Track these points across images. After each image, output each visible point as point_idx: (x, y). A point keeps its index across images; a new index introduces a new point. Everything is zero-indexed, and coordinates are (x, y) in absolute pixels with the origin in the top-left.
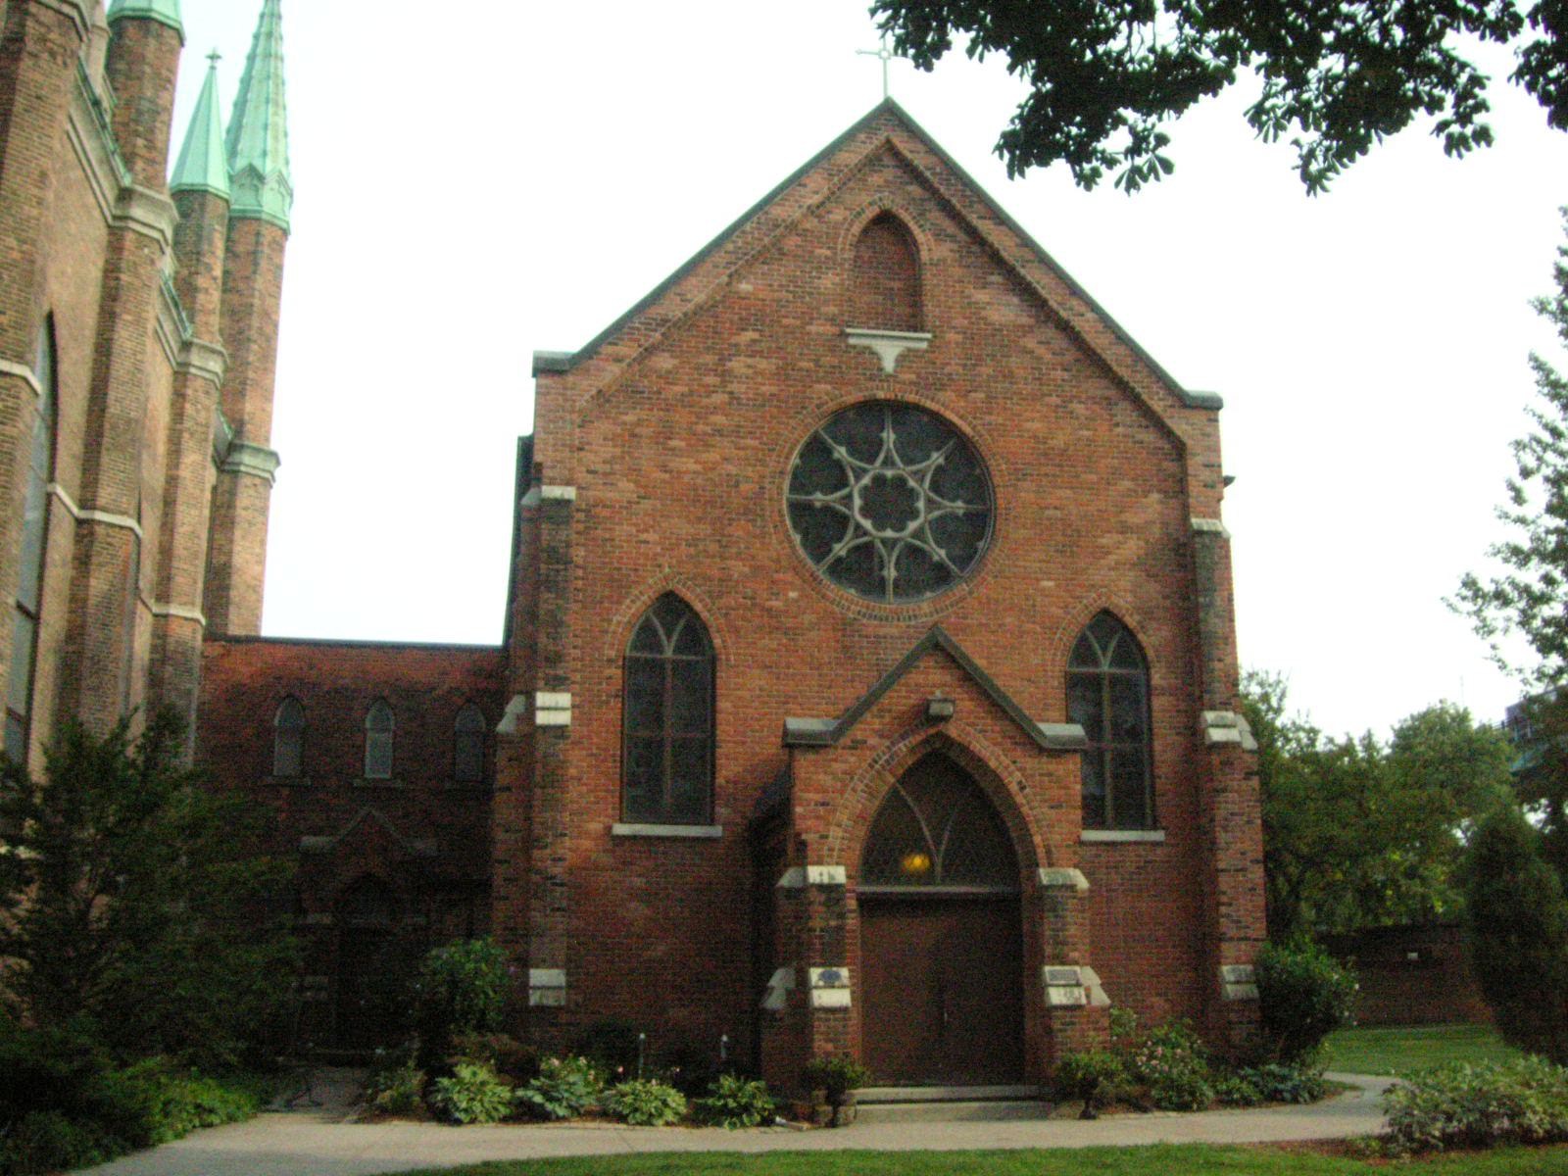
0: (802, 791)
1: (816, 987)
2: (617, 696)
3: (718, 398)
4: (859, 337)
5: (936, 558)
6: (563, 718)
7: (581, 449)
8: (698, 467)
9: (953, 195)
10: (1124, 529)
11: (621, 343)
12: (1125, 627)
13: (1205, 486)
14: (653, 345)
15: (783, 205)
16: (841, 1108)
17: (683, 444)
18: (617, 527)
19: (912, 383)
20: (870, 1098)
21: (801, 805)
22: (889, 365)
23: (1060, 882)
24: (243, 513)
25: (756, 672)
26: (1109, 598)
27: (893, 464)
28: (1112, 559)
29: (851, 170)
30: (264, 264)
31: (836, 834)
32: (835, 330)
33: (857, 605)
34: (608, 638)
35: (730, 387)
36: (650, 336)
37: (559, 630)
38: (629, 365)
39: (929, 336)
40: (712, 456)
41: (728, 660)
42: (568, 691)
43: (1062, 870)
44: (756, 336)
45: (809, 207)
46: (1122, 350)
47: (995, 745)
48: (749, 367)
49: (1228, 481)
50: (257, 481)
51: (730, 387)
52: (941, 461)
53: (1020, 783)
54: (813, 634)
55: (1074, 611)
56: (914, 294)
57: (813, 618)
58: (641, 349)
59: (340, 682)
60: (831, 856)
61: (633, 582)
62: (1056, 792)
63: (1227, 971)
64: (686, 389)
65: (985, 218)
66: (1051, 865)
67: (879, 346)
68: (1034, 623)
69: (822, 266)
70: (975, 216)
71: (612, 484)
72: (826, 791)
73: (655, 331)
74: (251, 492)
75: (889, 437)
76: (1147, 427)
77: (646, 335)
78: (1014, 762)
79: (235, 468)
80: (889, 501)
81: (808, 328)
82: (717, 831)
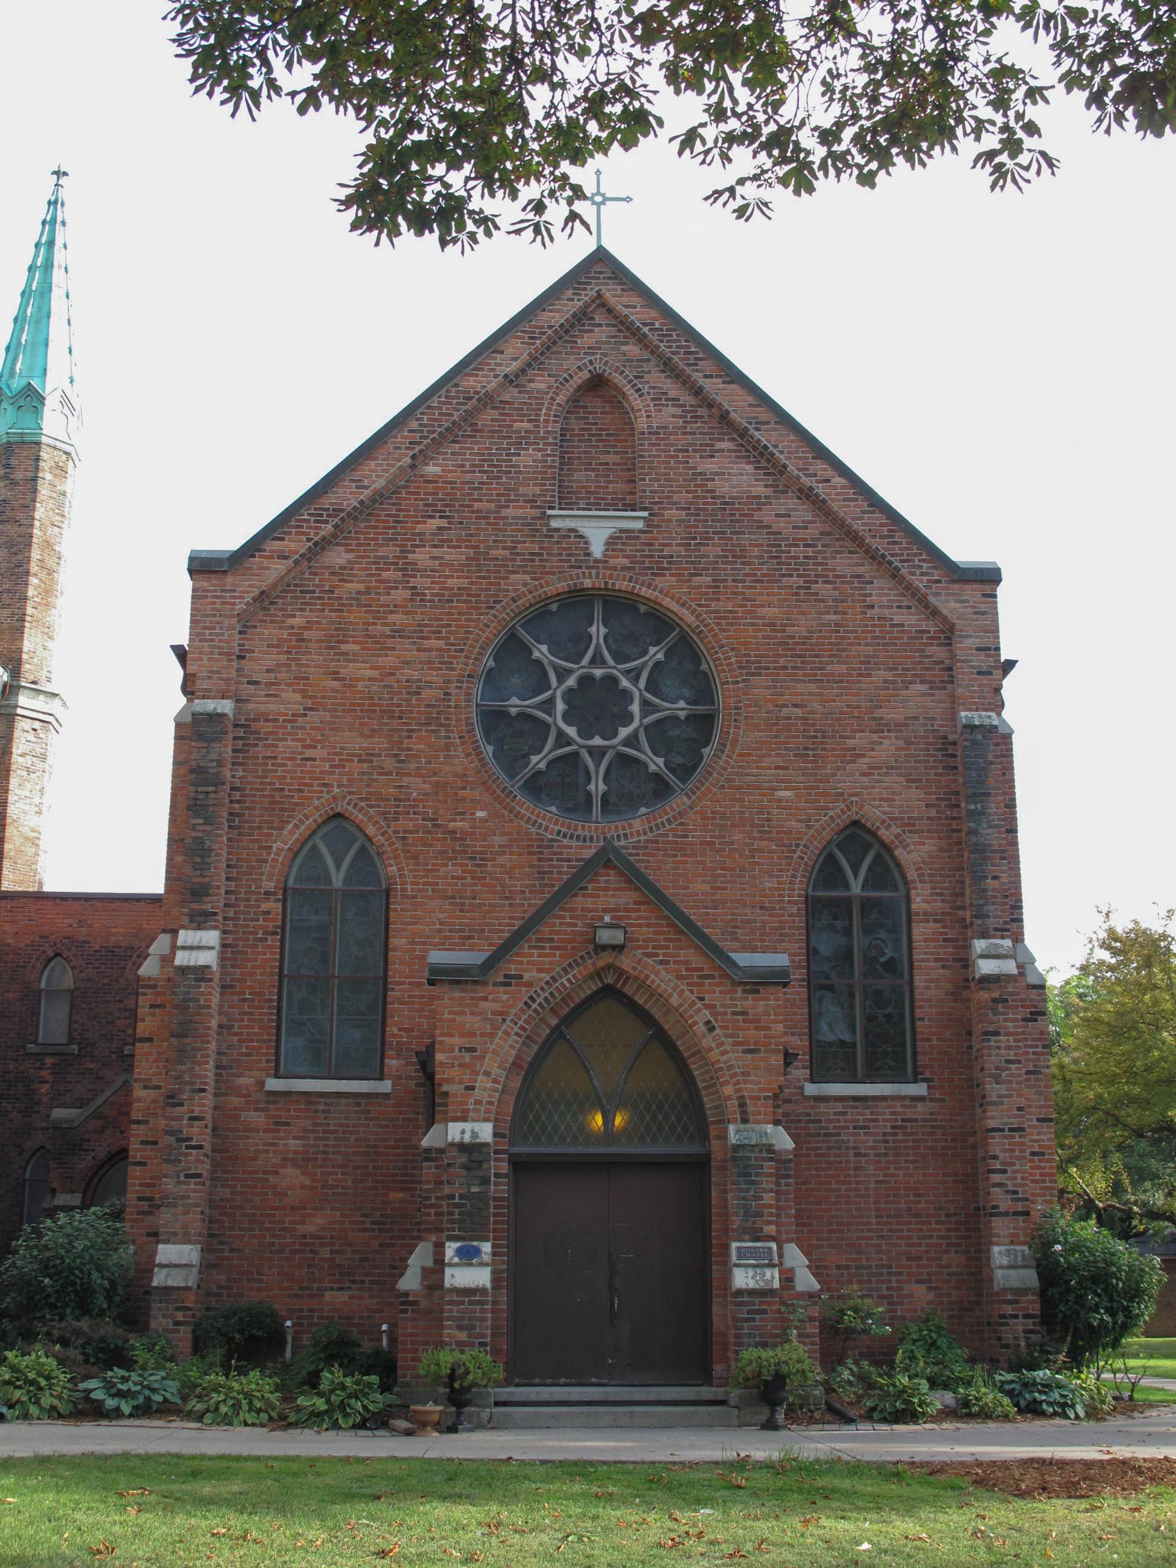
0: (443, 1035)
1: (451, 1265)
2: (276, 933)
3: (400, 595)
4: (561, 520)
5: (652, 768)
6: (208, 958)
7: (240, 658)
8: (376, 674)
9: (674, 353)
10: (881, 727)
11: (287, 537)
12: (882, 843)
13: (979, 673)
14: (324, 538)
15: (477, 375)
16: (466, 1410)
17: (357, 647)
18: (280, 744)
19: (624, 568)
20: (516, 1398)
21: (443, 1051)
22: (597, 549)
23: (753, 1142)
24: (20, 760)
25: (436, 903)
26: (861, 808)
27: (603, 662)
28: (862, 764)
29: (556, 332)
30: (44, 491)
31: (485, 1089)
32: (537, 512)
33: (556, 824)
34: (267, 868)
35: (413, 582)
36: (320, 528)
37: (207, 860)
38: (296, 562)
39: (646, 514)
40: (389, 660)
41: (404, 890)
42: (215, 928)
43: (756, 1127)
44: (443, 523)
45: (506, 376)
46: (879, 518)
47: (679, 977)
48: (435, 558)
49: (1010, 665)
50: (37, 725)
51: (413, 582)
52: (660, 656)
53: (708, 1023)
54: (501, 860)
55: (817, 825)
56: (630, 470)
57: (503, 840)
58: (310, 544)
59: (113, 939)
60: (477, 1111)
61: (296, 804)
62: (752, 1033)
63: (998, 1253)
64: (361, 587)
65: (711, 376)
66: (745, 1121)
67: (585, 528)
68: (769, 839)
69: (522, 441)
70: (701, 375)
71: (276, 696)
72: (473, 1035)
73: (327, 522)
74: (31, 736)
75: (598, 631)
76: (909, 607)
77: (316, 528)
78: (702, 999)
79: (11, 711)
81: (504, 512)
82: (386, 1086)
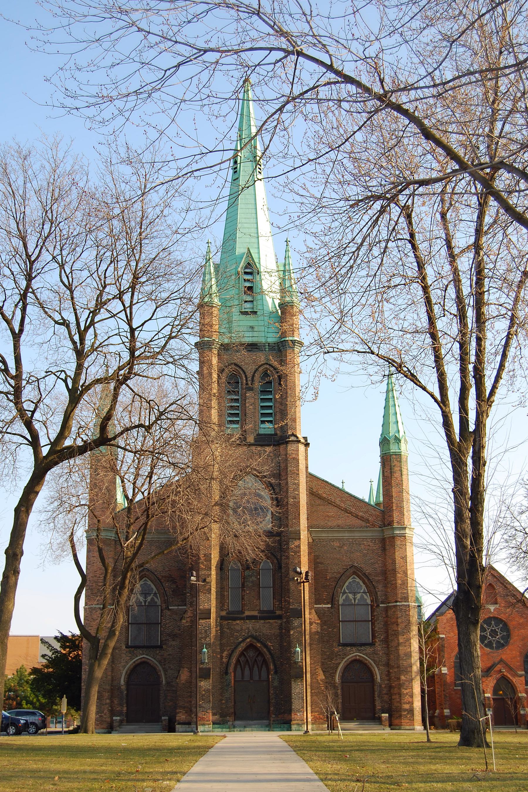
6: (446, 672)
80: (494, 633)
